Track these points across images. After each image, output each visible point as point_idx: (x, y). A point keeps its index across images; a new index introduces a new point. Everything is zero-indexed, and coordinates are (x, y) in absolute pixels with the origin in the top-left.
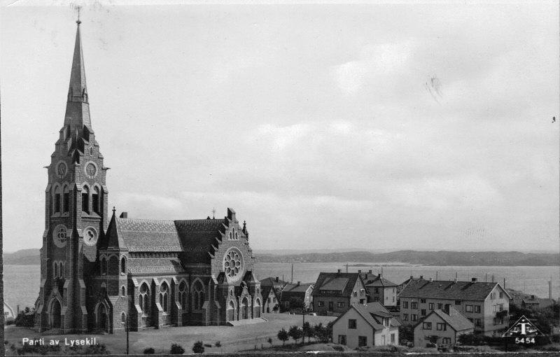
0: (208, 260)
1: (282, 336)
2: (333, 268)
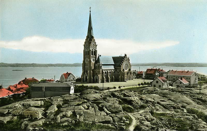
0: (120, 66)
1: (139, 85)
2: (150, 68)
